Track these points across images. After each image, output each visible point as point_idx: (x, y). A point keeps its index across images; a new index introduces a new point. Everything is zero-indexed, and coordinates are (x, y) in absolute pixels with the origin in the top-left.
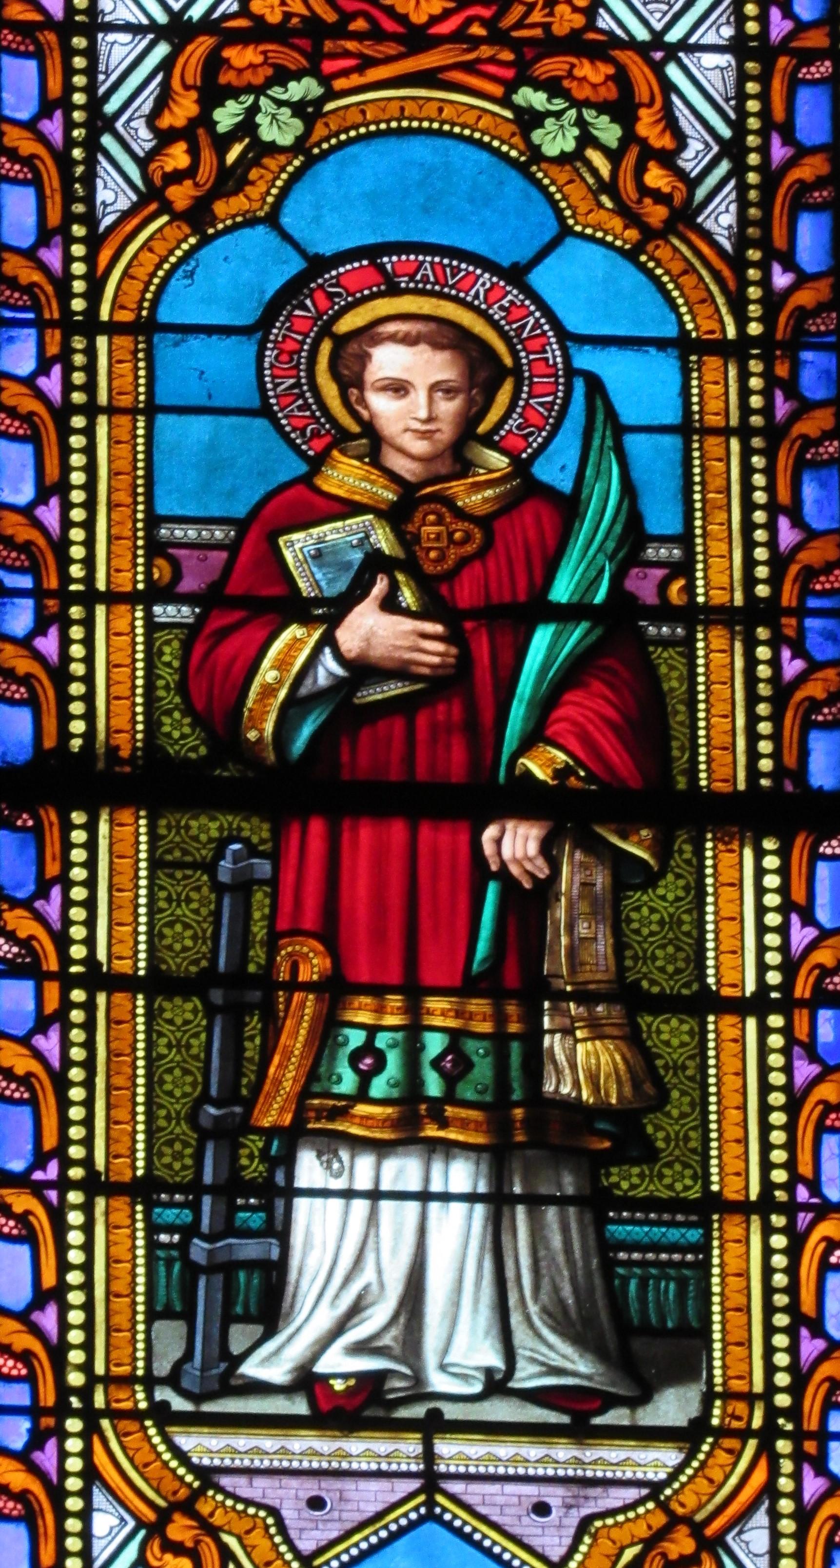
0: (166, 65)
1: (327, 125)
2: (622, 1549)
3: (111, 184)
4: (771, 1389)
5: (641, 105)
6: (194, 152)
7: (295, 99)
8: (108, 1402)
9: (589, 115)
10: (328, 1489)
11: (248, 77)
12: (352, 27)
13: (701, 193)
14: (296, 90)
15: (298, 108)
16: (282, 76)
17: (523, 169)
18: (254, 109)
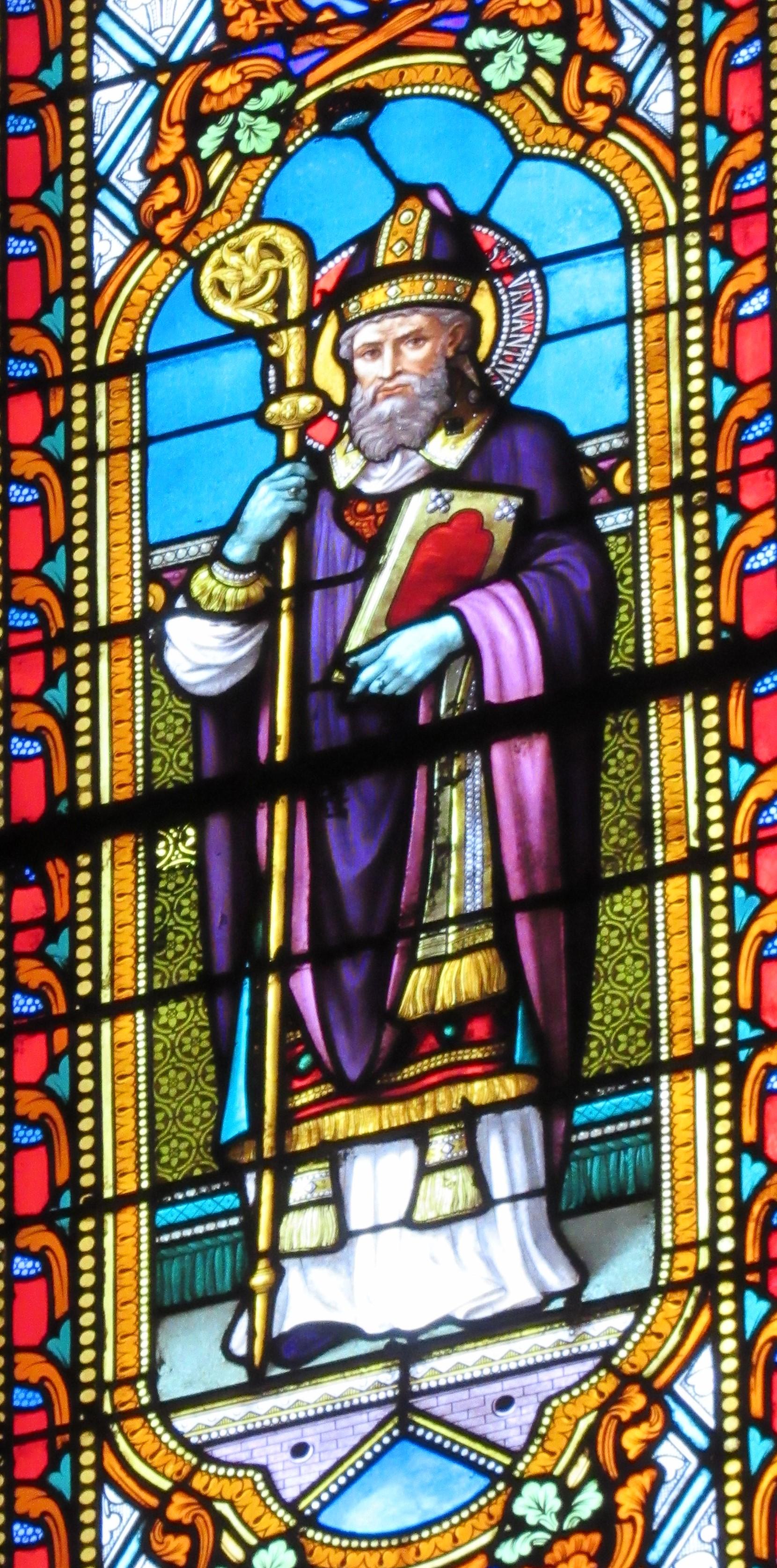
0: (155, 112)
1: (490, 1517)
2: (578, 1421)
3: (106, 235)
4: (715, 1235)
5: (582, 16)
6: (620, 1452)
7: (269, 105)
8: (114, 1407)
9: (534, 39)
10: (308, 1434)
11: (229, 99)
12: (321, 19)
13: (134, 1546)
14: (269, 97)
15: (519, 1526)
16: (259, 85)
17: (478, 107)
18: (562, 1515)
